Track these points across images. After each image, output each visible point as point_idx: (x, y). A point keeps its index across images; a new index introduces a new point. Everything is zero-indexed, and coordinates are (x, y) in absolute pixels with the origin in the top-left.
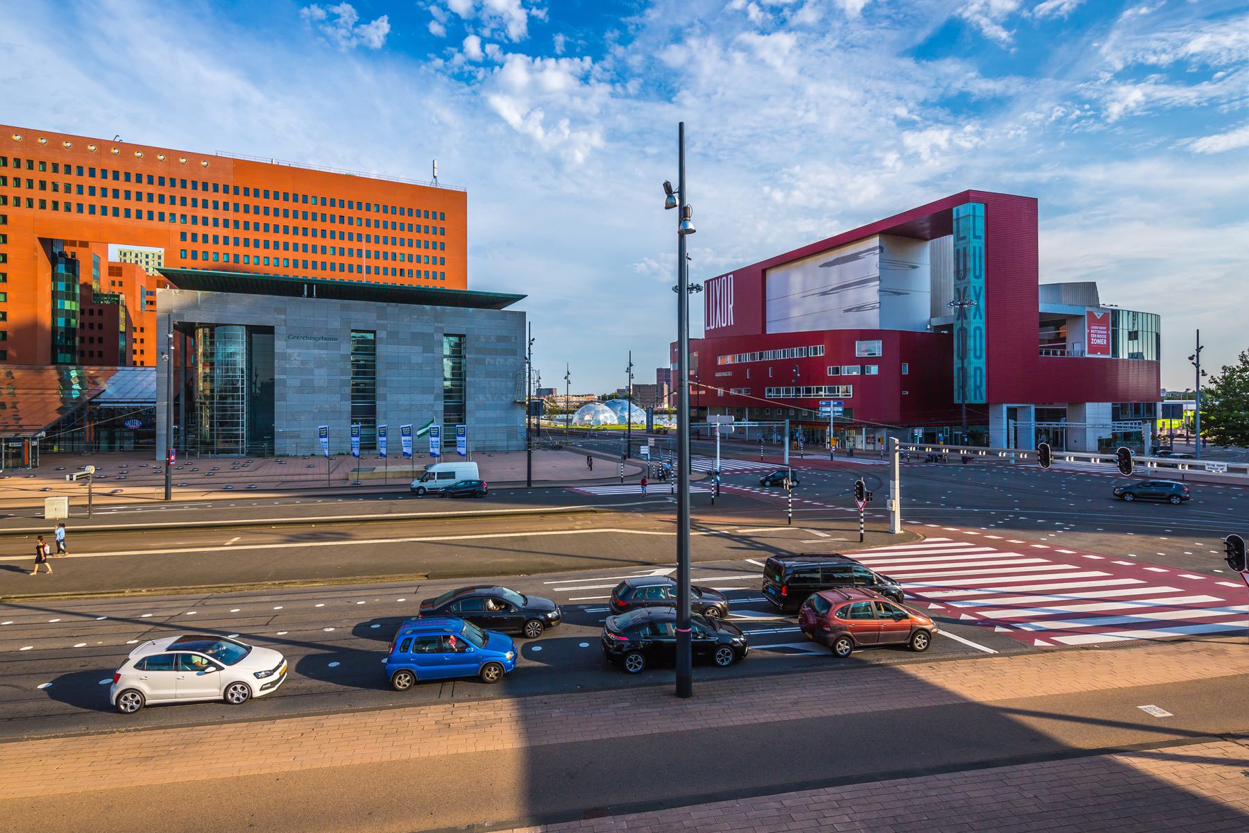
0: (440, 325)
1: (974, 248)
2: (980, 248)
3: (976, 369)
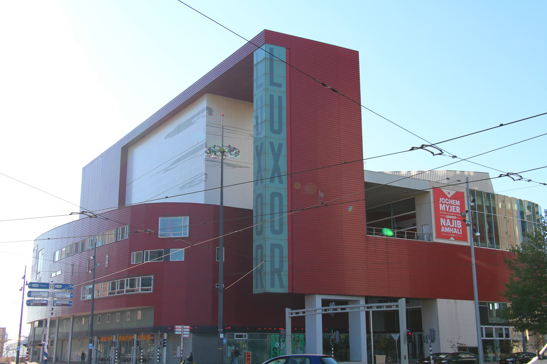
2: (280, 98)
3: (273, 246)
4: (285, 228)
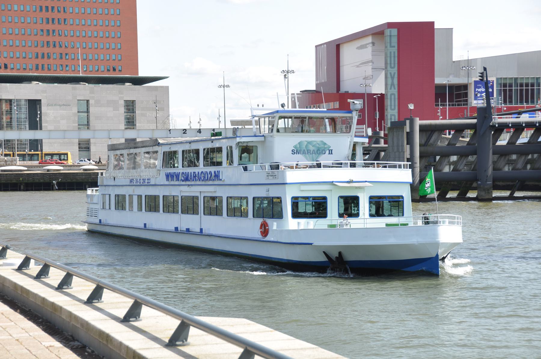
0: (122, 96)
1: (391, 53)
2: (394, 52)
3: (391, 115)
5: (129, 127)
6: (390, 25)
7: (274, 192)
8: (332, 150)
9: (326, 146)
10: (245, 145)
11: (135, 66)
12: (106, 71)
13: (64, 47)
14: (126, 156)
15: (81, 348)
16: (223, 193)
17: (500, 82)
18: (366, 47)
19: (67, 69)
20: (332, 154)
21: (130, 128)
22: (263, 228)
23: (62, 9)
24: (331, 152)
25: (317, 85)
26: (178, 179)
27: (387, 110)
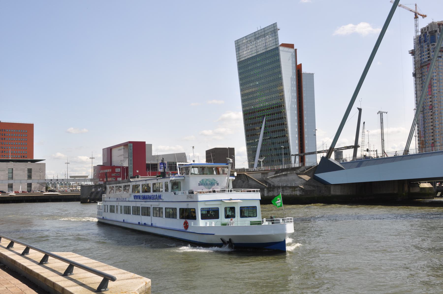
0: (26, 167)
1: (130, 152)
2: (132, 152)
4: (132, 156)
5: (29, 178)
6: (130, 142)
7: (191, 206)
8: (218, 183)
9: (215, 181)
10: (174, 181)
11: (32, 155)
12: (20, 157)
13: (3, 148)
14: (115, 187)
15: (3, 266)
16: (163, 206)
17: (168, 163)
18: (121, 150)
19: (5, 157)
20: (218, 185)
21: (29, 179)
22: (185, 225)
23: (4, 135)
24: (218, 184)
25: (103, 163)
26: (140, 198)
27: (129, 172)
